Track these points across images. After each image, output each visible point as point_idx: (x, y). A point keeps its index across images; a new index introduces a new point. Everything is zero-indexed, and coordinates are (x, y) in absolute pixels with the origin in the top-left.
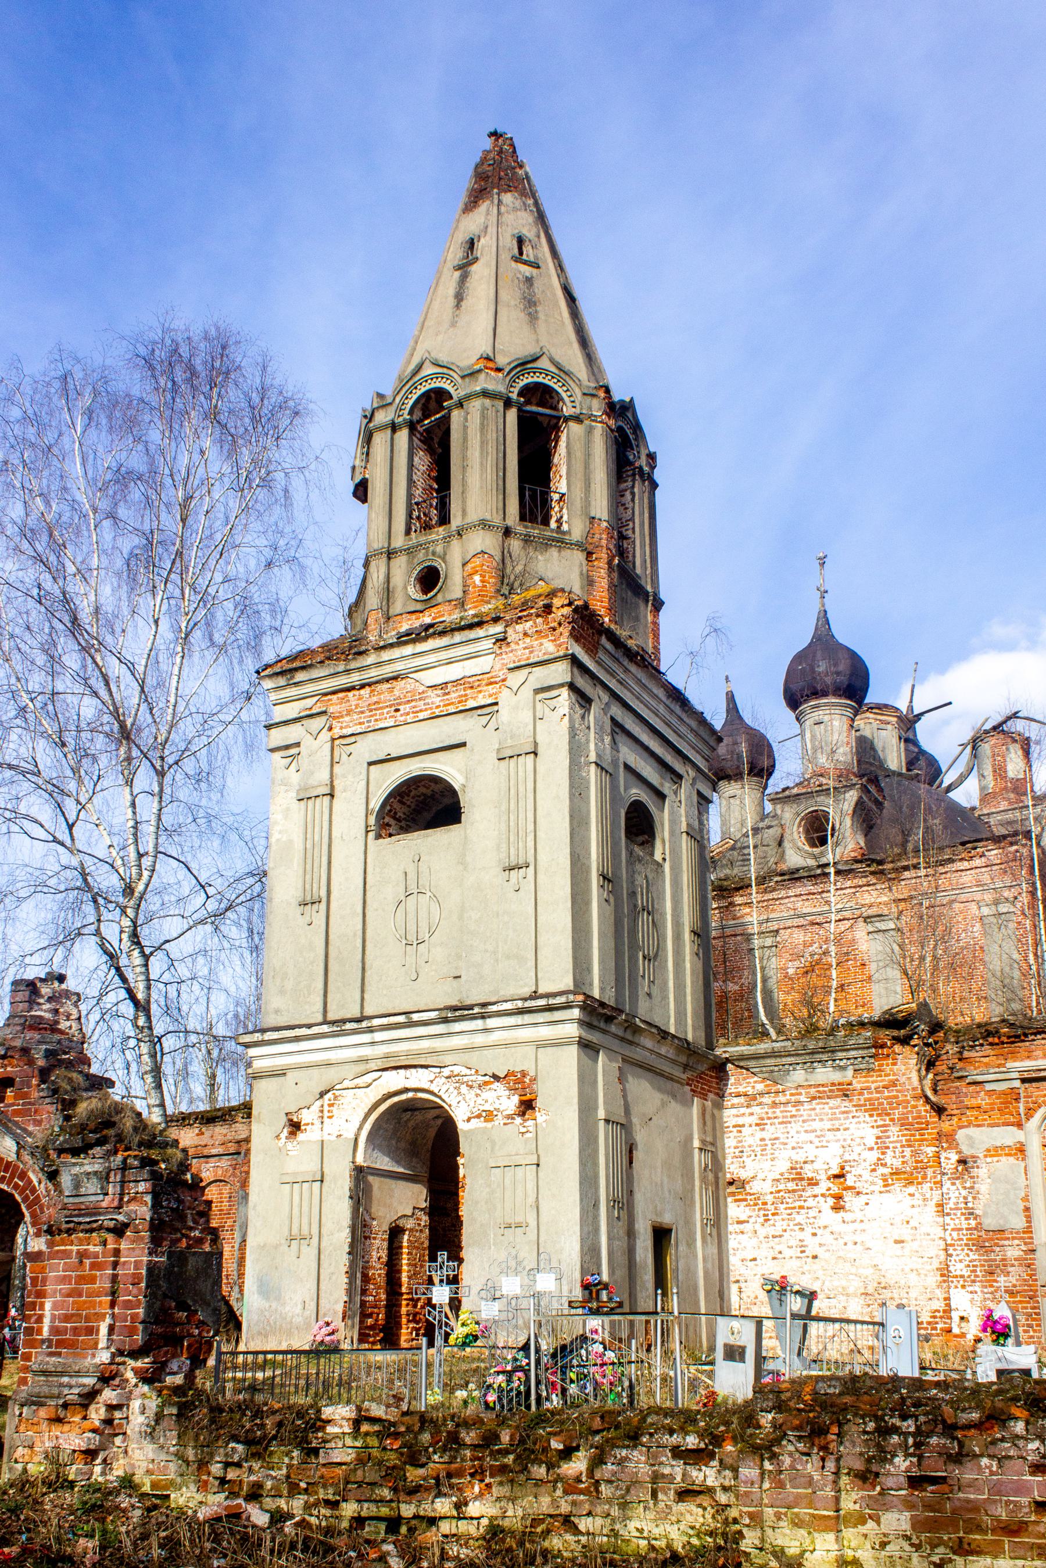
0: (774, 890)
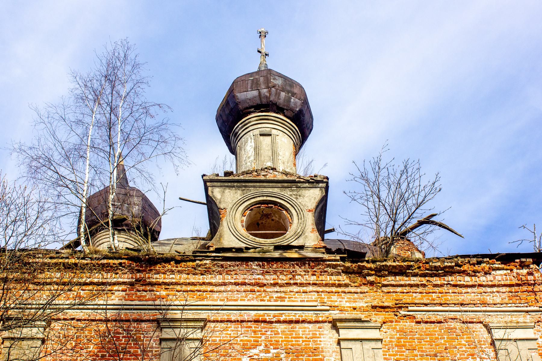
0: (207, 271)
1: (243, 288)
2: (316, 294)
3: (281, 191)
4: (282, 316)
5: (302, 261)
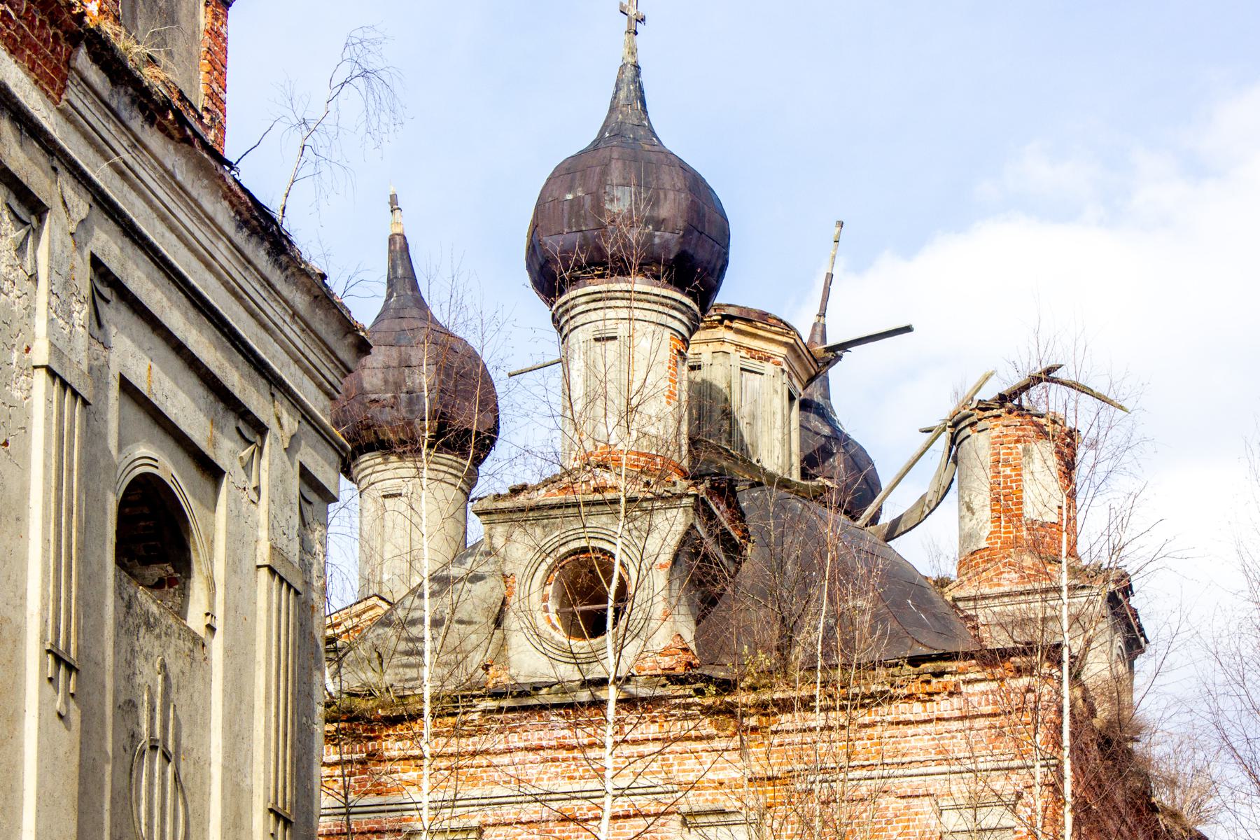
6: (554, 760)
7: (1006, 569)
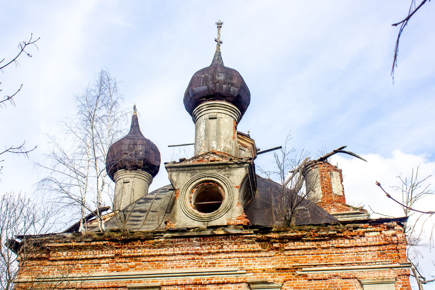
0: (162, 246)
1: (188, 257)
2: (237, 259)
3: (218, 172)
4: (213, 280)
5: (227, 235)
6: (193, 259)
7: (332, 207)
